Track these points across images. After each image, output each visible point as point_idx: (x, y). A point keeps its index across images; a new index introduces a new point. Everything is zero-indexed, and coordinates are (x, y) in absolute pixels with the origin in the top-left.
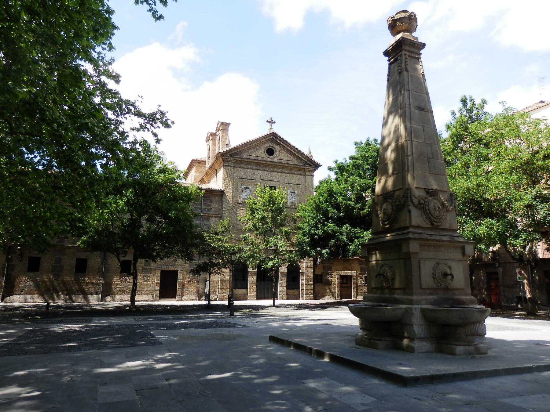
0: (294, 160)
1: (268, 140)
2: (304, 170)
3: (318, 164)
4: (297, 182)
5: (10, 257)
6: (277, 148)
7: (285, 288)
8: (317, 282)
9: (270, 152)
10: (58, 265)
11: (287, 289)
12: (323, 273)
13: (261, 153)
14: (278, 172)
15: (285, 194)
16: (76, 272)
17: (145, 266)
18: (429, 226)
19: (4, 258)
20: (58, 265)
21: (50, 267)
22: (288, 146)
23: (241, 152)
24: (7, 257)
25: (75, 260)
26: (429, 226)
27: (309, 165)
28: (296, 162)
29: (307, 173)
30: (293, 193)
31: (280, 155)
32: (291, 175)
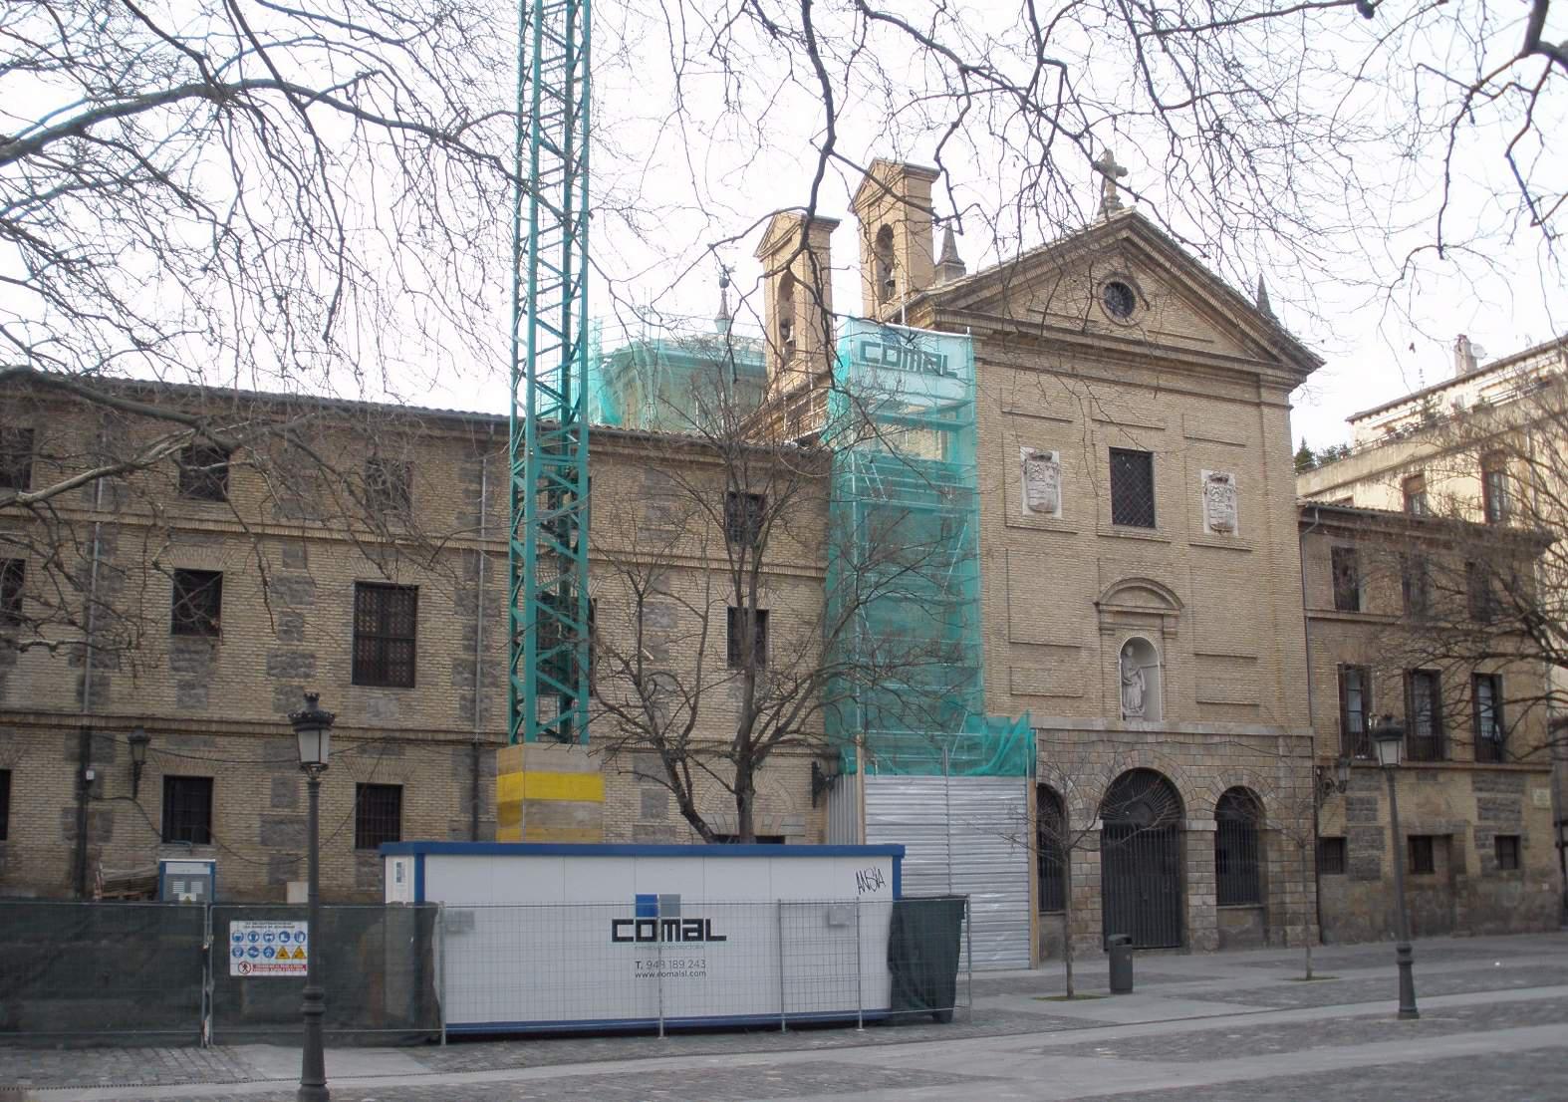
0: (1214, 336)
1: (1107, 251)
2: (1256, 381)
3: (1152, 516)
4: (1228, 433)
5: (90, 775)
6: (1146, 283)
7: (1212, 900)
8: (1326, 871)
9: (1122, 297)
10: (287, 811)
11: (1219, 902)
12: (1346, 830)
13: (1077, 305)
14: (1158, 389)
15: (755, 401)
16: (357, 846)
17: (644, 815)
18: (560, 330)
19: (70, 780)
20: (287, 811)
21: (256, 824)
22: (1189, 274)
23: (1006, 296)
24: (81, 774)
25: (353, 791)
26: (560, 330)
27: (1272, 360)
28: (1221, 346)
29: (1266, 395)
30: (1220, 480)
31: (1163, 320)
32: (1204, 403)
